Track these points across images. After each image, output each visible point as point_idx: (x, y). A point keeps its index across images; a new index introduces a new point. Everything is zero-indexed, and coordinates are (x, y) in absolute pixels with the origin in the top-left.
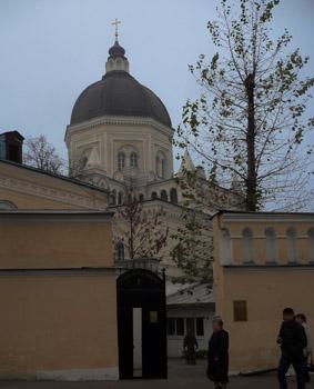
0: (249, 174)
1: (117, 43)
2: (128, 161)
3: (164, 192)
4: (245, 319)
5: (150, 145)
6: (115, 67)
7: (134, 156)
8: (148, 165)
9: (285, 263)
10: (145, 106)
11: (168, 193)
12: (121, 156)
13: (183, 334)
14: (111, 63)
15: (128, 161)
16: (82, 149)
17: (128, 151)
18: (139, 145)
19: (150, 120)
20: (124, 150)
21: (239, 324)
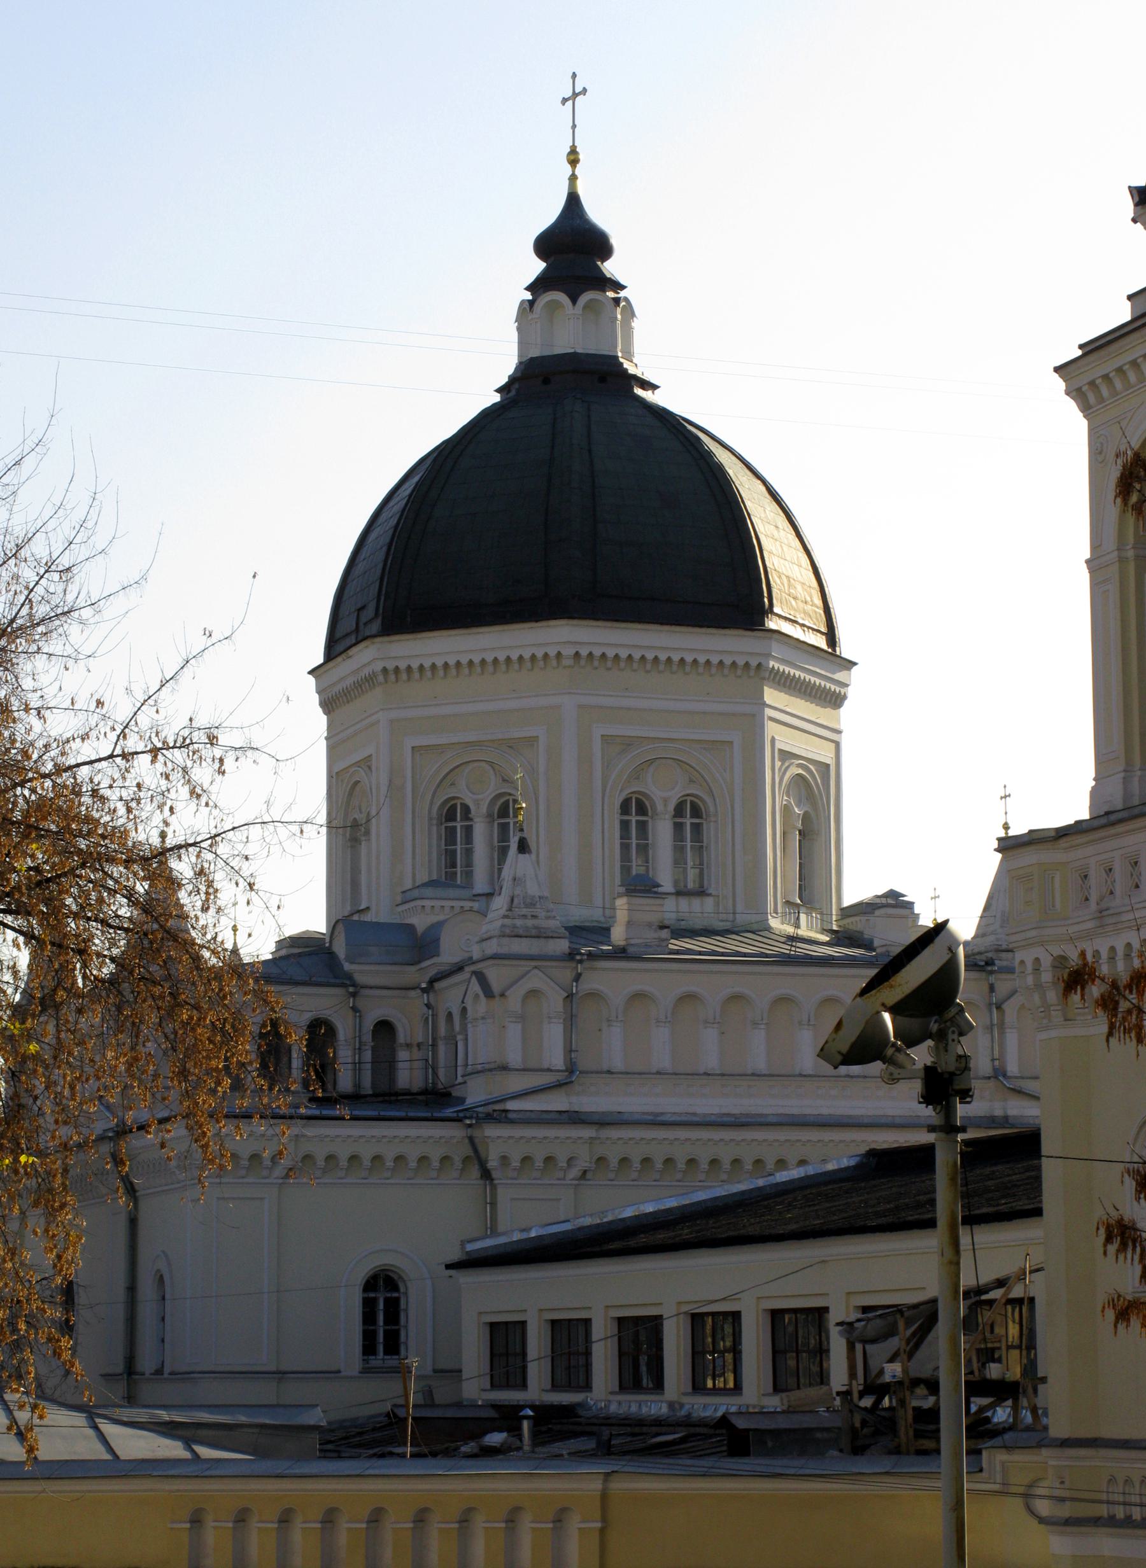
1: (573, 202)
2: (662, 831)
15: (662, 831)
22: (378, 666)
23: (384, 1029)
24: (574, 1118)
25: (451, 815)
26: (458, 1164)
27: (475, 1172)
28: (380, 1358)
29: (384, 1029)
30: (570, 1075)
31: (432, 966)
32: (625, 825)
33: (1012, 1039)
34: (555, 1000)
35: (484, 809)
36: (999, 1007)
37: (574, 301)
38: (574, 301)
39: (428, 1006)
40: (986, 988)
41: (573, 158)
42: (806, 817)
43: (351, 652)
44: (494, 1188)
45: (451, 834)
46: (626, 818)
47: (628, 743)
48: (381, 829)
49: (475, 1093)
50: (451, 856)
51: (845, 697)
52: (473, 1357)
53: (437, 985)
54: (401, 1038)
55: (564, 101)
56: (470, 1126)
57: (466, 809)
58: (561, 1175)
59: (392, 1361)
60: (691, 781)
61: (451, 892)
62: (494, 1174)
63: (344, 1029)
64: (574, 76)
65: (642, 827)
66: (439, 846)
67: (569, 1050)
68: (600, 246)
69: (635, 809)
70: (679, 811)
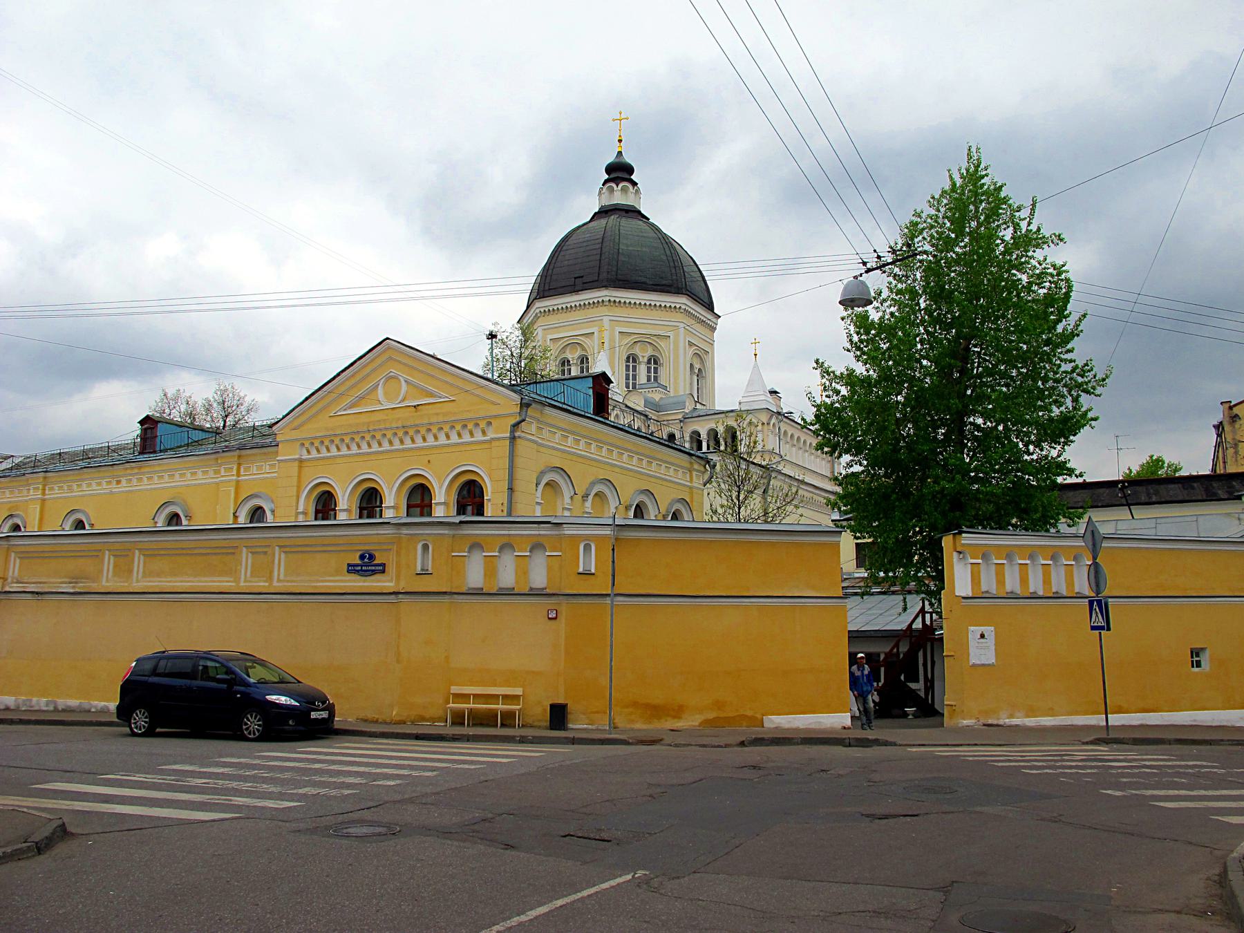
0: (943, 372)
1: (620, 153)
2: (642, 370)
3: (713, 434)
4: (552, 706)
5: (681, 345)
6: (619, 197)
7: (654, 361)
8: (676, 380)
9: (431, 703)
10: (671, 275)
11: (704, 436)
12: (632, 359)
13: (878, 680)
14: (611, 190)
15: (642, 370)
16: (561, 344)
17: (643, 354)
18: (662, 344)
19: (682, 301)
20: (637, 351)
21: (561, 701)
32: (628, 367)
65: (635, 368)
70: (649, 362)
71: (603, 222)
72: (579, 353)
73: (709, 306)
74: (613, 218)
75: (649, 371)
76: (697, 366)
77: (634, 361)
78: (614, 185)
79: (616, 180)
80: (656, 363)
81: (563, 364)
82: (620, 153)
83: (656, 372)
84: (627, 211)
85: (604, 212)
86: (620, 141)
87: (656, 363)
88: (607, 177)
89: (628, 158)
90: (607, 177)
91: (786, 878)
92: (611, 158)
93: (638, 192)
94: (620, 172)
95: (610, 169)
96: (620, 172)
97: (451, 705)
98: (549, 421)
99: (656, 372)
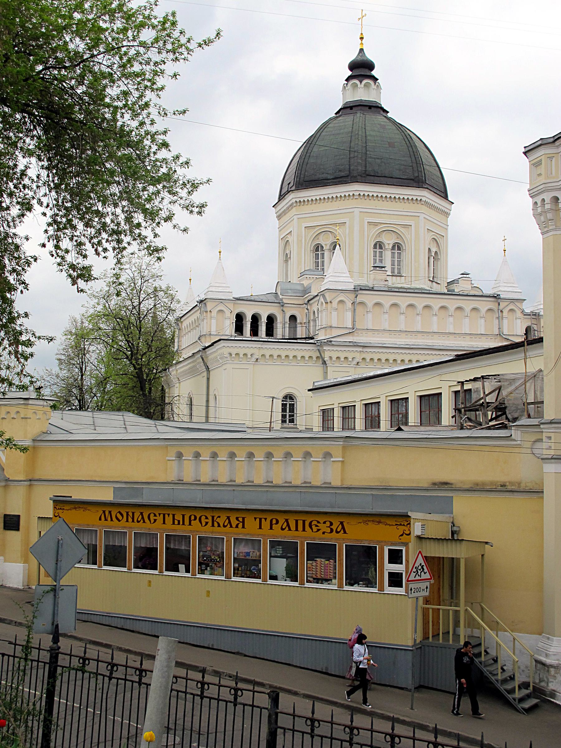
1: (361, 50)
2: (388, 255)
6: (362, 93)
7: (397, 247)
10: (408, 167)
15: (388, 255)
16: (317, 230)
17: (389, 241)
22: (294, 200)
23: (293, 318)
24: (355, 345)
25: (317, 250)
26: (315, 359)
27: (321, 361)
28: (288, 424)
29: (293, 318)
30: (353, 331)
31: (308, 296)
33: (505, 321)
34: (349, 305)
35: (328, 247)
36: (501, 311)
37: (361, 82)
38: (361, 82)
39: (307, 309)
40: (497, 304)
41: (362, 38)
42: (436, 252)
43: (285, 197)
44: (327, 367)
45: (317, 255)
46: (375, 250)
47: (376, 224)
48: (294, 256)
49: (321, 336)
50: (288, 208)
51: (449, 214)
52: (316, 422)
53: (311, 302)
54: (298, 321)
55: (359, 19)
56: (318, 345)
57: (322, 247)
58: (349, 363)
59: (291, 425)
60: (398, 238)
61: (316, 273)
62: (327, 363)
63: (279, 319)
64: (362, 10)
66: (313, 260)
67: (354, 321)
68: (370, 66)
69: (379, 245)
70: (393, 248)
71: (348, 119)
72: (331, 239)
73: (445, 196)
74: (359, 115)
75: (393, 257)
76: (434, 250)
77: (381, 247)
78: (357, 82)
79: (361, 77)
80: (399, 249)
81: (317, 250)
82: (361, 50)
83: (399, 257)
84: (370, 107)
85: (349, 108)
86: (362, 38)
87: (399, 249)
88: (350, 73)
89: (370, 56)
90: (350, 73)
91: (413, 664)
92: (353, 56)
93: (379, 87)
94: (362, 69)
95: (353, 66)
96: (362, 69)
97: (451, 642)
98: (26, 483)
99: (399, 257)
